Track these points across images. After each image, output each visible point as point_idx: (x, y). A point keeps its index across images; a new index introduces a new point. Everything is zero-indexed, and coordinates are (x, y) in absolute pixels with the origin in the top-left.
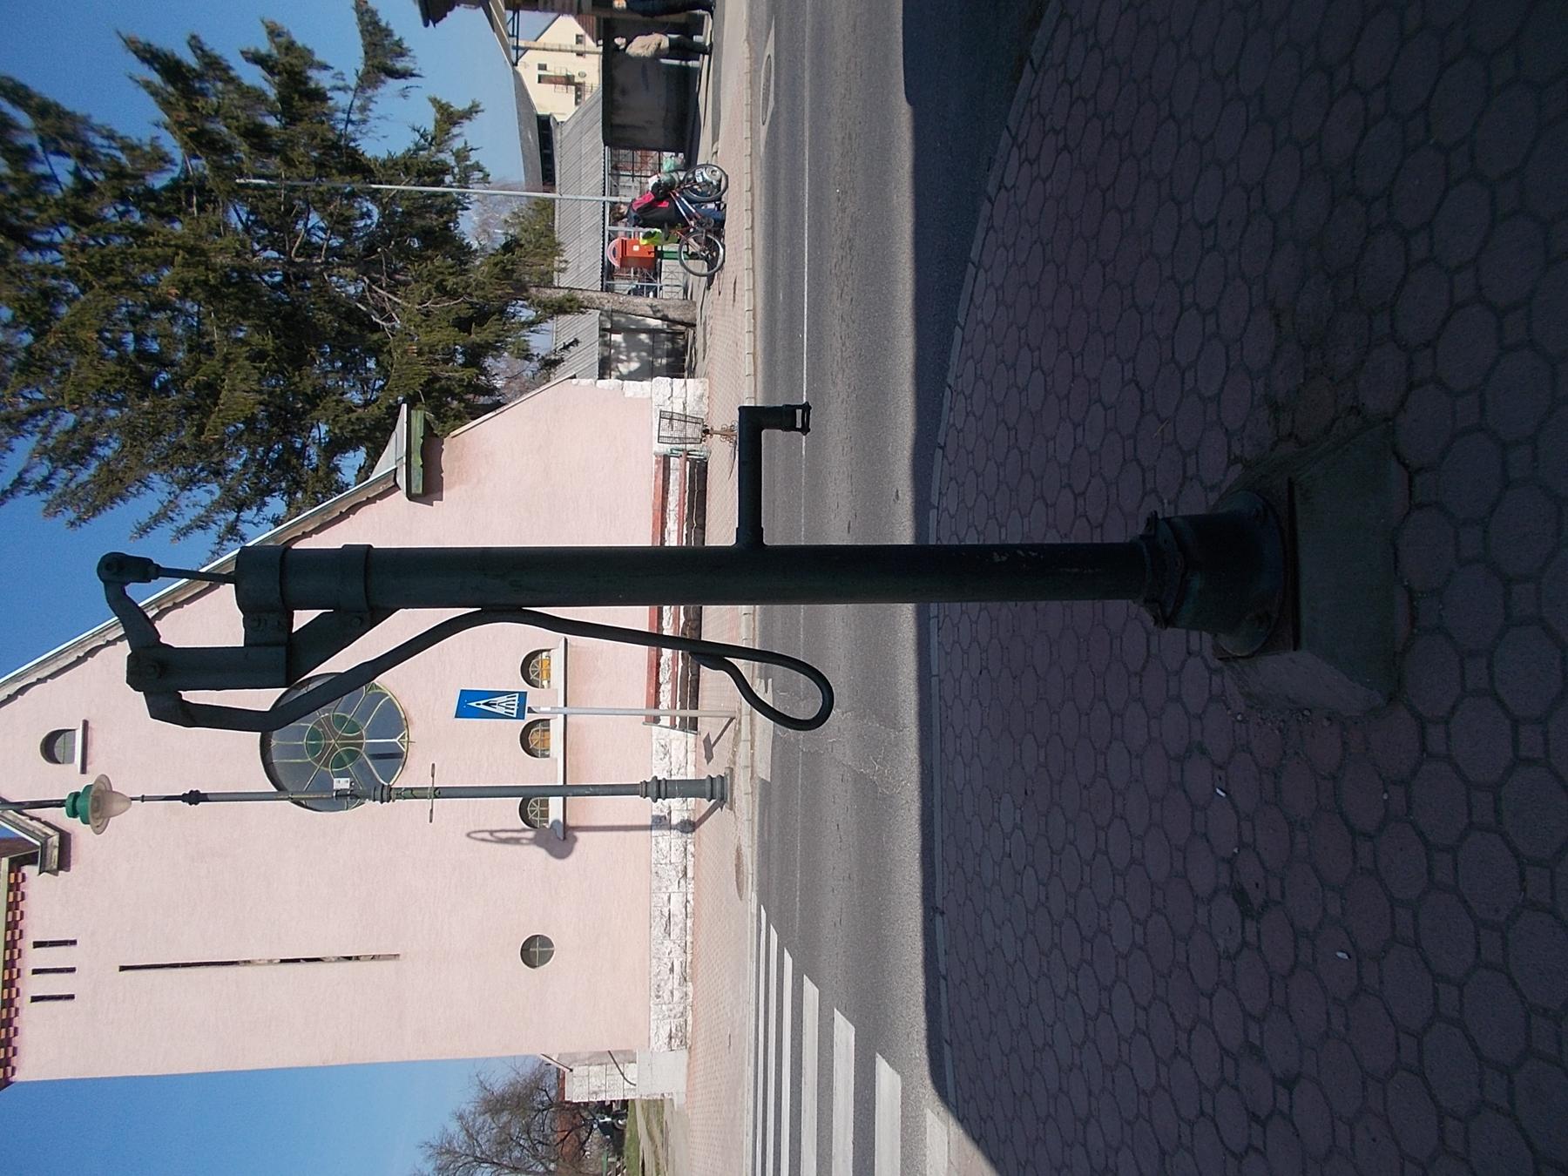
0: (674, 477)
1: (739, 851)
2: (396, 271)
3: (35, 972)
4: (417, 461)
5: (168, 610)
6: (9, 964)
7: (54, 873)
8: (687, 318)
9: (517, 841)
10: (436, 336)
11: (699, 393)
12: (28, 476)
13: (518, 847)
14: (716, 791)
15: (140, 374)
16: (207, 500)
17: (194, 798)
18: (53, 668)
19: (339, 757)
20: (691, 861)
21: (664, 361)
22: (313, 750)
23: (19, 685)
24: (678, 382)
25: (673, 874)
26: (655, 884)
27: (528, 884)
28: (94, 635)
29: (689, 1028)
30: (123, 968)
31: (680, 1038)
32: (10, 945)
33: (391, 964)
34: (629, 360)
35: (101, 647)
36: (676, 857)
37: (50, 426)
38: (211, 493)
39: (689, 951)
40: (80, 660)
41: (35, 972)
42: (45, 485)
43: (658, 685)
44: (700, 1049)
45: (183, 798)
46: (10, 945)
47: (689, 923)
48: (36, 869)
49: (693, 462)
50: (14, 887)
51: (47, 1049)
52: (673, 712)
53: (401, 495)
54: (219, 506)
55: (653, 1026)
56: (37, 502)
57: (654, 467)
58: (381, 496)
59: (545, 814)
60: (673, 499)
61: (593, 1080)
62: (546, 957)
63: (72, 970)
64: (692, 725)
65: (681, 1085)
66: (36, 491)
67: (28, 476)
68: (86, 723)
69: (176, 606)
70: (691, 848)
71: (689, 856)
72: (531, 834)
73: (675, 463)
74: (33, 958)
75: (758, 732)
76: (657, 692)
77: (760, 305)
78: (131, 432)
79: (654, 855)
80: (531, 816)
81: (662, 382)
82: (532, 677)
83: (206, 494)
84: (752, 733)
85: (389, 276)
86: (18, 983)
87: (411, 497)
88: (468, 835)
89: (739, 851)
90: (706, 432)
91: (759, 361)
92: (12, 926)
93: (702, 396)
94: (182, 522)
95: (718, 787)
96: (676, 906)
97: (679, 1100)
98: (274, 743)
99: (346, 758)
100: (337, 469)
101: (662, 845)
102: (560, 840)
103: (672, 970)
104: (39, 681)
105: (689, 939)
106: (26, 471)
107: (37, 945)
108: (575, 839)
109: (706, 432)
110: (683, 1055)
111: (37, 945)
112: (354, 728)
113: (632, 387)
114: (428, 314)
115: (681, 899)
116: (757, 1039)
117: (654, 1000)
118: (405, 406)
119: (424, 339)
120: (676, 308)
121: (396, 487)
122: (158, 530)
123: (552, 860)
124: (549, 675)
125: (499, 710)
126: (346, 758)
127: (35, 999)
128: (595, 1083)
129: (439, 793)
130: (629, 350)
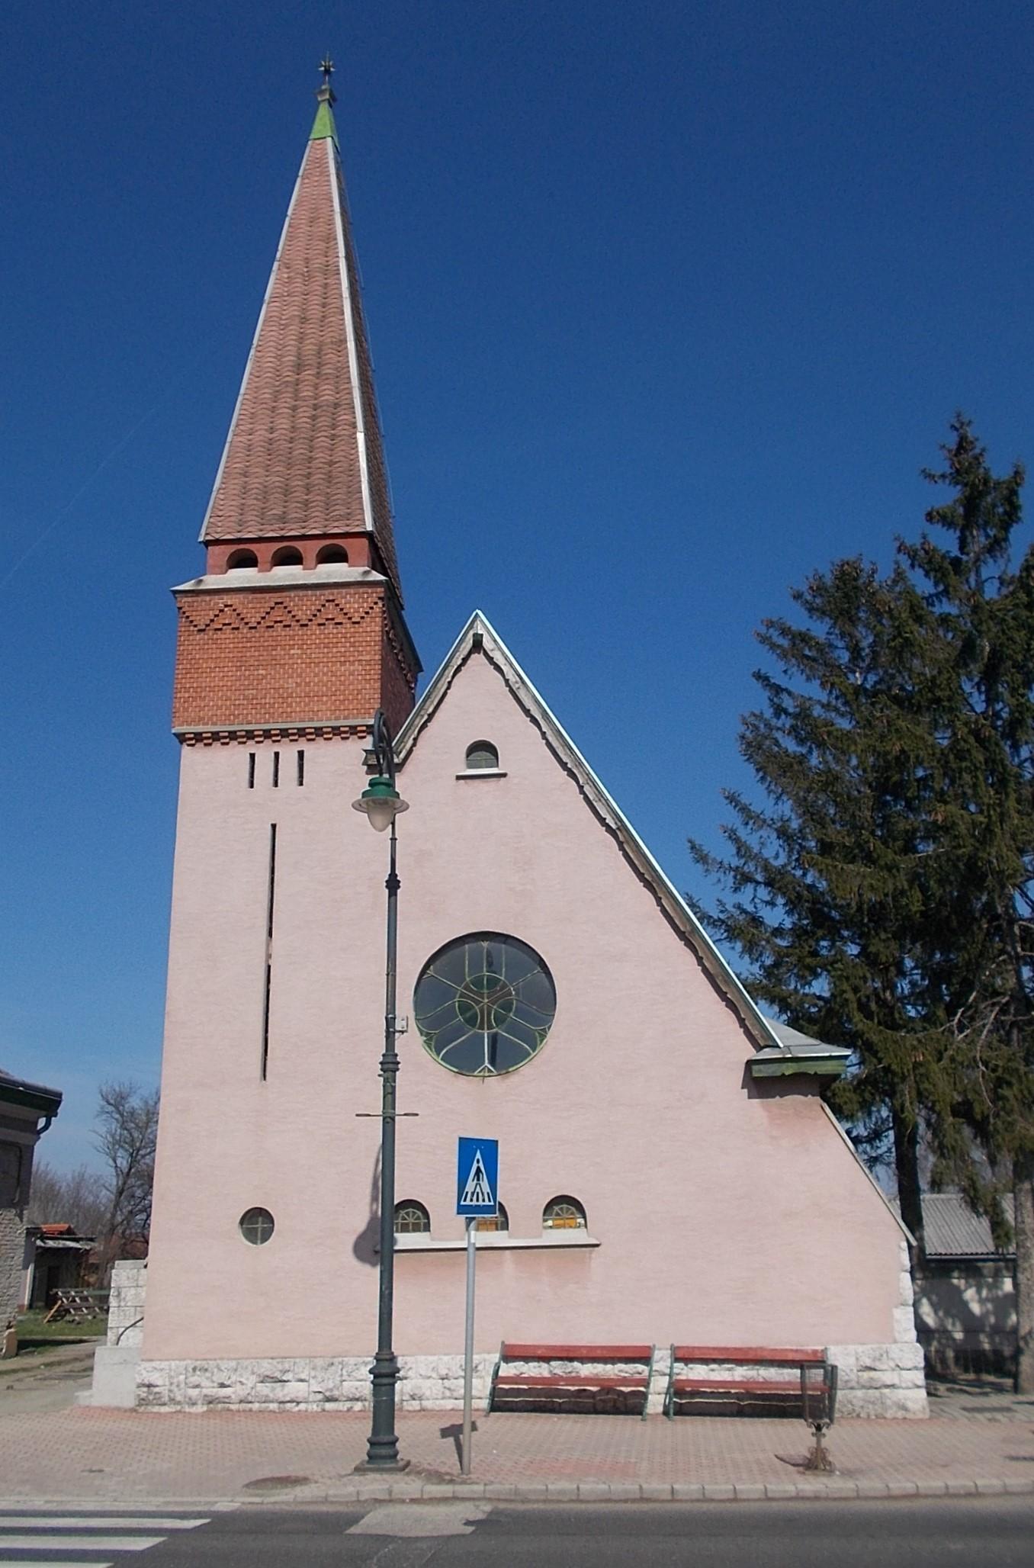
2: (1020, 1030)
3: (277, 754)
4: (789, 1069)
5: (616, 837)
6: (284, 733)
11: (909, 1405)
12: (784, 696)
13: (368, 1199)
14: (382, 1449)
15: (890, 782)
16: (768, 853)
17: (393, 884)
19: (470, 1008)
20: (343, 1406)
21: (987, 1346)
22: (478, 982)
23: (539, 717)
24: (919, 1377)
26: (319, 1362)
28: (588, 774)
29: (156, 1409)
30: (274, 826)
31: (149, 1395)
32: (302, 733)
33: (259, 1072)
34: (981, 1301)
35: (577, 782)
36: (349, 1387)
37: (836, 710)
38: (777, 856)
39: (243, 1406)
40: (564, 765)
41: (277, 754)
42: (779, 711)
43: (547, 1359)
46: (302, 733)
47: (273, 1406)
48: (370, 748)
50: (354, 730)
51: (207, 775)
53: (751, 1053)
54: (766, 867)
55: (164, 1365)
57: (810, 1348)
58: (748, 1034)
59: (405, 1229)
61: (133, 1291)
62: (266, 1235)
63: (276, 784)
64: (499, 1403)
65: (96, 1402)
67: (784, 696)
68: (504, 775)
69: (620, 844)
70: (358, 1406)
71: (348, 1404)
74: (289, 752)
75: (417, 1509)
77: (978, 1504)
78: (830, 781)
79: (352, 1361)
81: (915, 1355)
82: (556, 1208)
85: (1013, 1024)
86: (268, 742)
87: (750, 1064)
92: (319, 732)
93: (905, 1408)
94: (743, 833)
95: (383, 1451)
96: (294, 1389)
97: (84, 1397)
98: (485, 944)
99: (468, 1015)
100: (816, 976)
103: (222, 1385)
104: (543, 734)
105: (256, 1406)
106: (790, 693)
107: (301, 754)
108: (374, 1265)
110: (130, 1402)
111: (301, 754)
112: (500, 1020)
113: (905, 1319)
117: (191, 1364)
121: (759, 1048)
122: (734, 813)
124: (558, 1227)
125: (470, 1186)
126: (468, 1015)
129: (389, 1122)
130: (995, 1300)
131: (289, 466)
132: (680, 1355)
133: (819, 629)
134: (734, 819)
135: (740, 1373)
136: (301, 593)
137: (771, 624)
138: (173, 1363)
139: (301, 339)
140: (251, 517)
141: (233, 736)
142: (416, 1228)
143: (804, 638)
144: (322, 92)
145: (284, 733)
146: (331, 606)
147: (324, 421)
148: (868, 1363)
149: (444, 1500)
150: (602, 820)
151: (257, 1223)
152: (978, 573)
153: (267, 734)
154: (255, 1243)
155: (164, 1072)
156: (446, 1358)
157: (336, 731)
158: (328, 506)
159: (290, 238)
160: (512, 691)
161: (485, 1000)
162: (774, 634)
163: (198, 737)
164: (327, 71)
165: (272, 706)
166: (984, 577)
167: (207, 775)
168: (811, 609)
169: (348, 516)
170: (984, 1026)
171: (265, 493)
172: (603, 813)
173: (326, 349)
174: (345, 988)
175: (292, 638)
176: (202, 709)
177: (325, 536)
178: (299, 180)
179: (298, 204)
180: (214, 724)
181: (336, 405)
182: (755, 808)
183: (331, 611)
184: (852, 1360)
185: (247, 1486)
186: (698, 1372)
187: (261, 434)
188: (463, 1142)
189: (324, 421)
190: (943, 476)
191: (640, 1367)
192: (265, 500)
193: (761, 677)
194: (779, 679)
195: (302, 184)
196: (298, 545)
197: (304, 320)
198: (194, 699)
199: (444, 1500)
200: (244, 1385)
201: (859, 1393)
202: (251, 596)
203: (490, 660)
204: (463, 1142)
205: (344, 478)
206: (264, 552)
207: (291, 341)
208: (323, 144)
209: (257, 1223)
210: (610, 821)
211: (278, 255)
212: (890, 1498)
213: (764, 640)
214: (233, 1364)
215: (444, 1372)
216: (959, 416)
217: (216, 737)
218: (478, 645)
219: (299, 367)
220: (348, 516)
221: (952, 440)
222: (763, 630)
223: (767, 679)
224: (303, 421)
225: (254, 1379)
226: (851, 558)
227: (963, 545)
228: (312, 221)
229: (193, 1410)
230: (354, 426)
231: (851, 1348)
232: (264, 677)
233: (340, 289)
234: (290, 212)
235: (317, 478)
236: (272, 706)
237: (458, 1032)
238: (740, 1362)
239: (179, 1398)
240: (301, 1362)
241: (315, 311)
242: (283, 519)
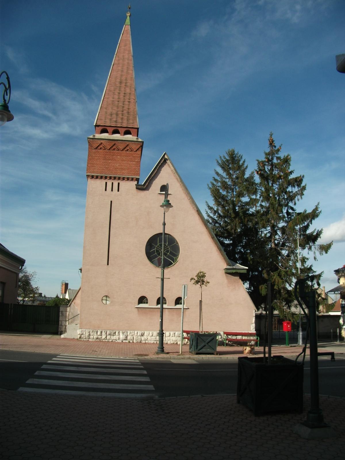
4: (234, 271)
32: (119, 178)
92: (124, 179)
129: (163, 280)
139: (122, 75)
219: (121, 83)
235: (125, 112)
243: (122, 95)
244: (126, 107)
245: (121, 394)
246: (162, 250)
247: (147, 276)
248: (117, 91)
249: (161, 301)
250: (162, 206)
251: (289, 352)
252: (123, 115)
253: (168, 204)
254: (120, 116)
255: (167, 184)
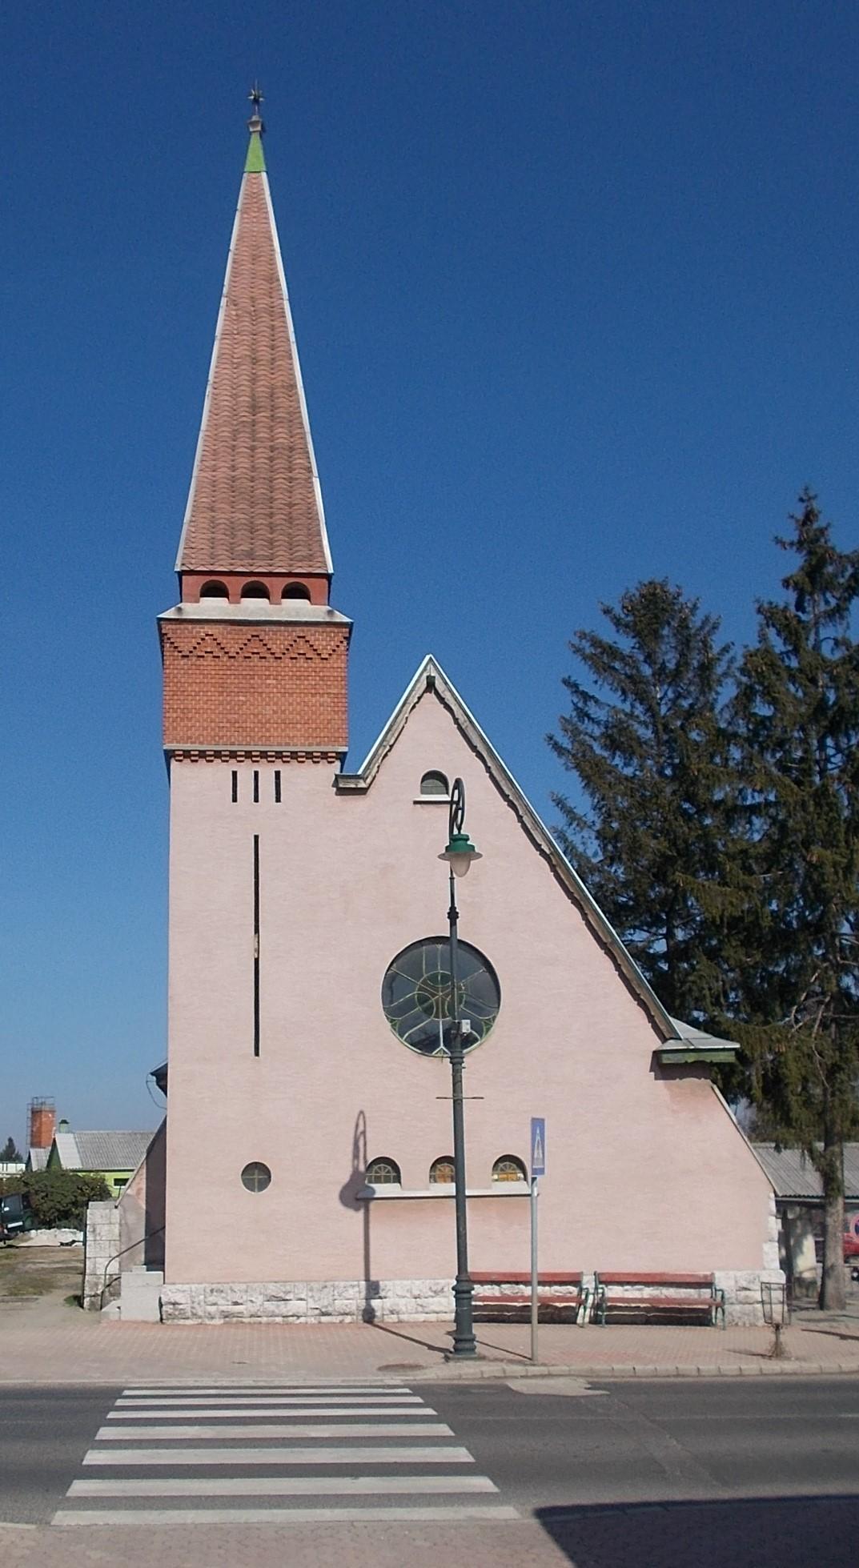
0: (692, 1293)
1: (417, 1367)
2: (838, 1026)
3: (256, 773)
4: (691, 1058)
6: (264, 755)
7: (336, 784)
8: (829, 1300)
9: (356, 1156)
10: (792, 1065)
12: (591, 703)
13: (350, 1156)
18: (498, 778)
20: (336, 1319)
22: (433, 978)
23: (485, 755)
25: (324, 1303)
26: (315, 1286)
27: (317, 1168)
28: (526, 806)
29: (182, 1322)
31: (166, 1314)
32: (279, 755)
40: (505, 797)
41: (256, 773)
43: (498, 1283)
44: (161, 1333)
45: (453, 908)
46: (279, 755)
47: (279, 1319)
49: (708, 1312)
50: (325, 756)
51: (195, 787)
52: (535, 1299)
53: (656, 1044)
55: (186, 1287)
56: (569, 712)
57: (702, 1273)
58: (656, 1027)
59: (378, 1180)
60: (683, 1293)
61: (106, 1228)
62: (249, 1184)
66: (577, 708)
67: (591, 703)
69: (553, 868)
70: (348, 1319)
71: (340, 1318)
72: (362, 1168)
73: (706, 1293)
74: (267, 771)
76: (492, 1283)
79: (342, 1284)
80: (376, 1167)
83: (593, 849)
84: (534, 1376)
87: (657, 1054)
88: (362, 1112)
89: (417, 1367)
90: (777, 1327)
91: (672, 1380)
92: (294, 755)
94: (569, 834)
95: (467, 1345)
98: (440, 946)
101: (351, 1291)
102: (357, 1196)
103: (236, 1303)
105: (264, 1320)
106: (597, 701)
107: (278, 774)
108: (357, 1209)
109: (777, 1327)
111: (278, 774)
114: (810, 1057)
115: (301, 1311)
116: (198, 1388)
118: (737, 1046)
119: (790, 1056)
120: (837, 1289)
121: (664, 1039)
123: (339, 1188)
124: (504, 1180)
127: (235, 774)
128: (103, 1230)
129: (458, 1104)
131: (252, 504)
132: (603, 1279)
133: (626, 643)
134: (561, 820)
135: (648, 1292)
136: (275, 628)
137: (583, 636)
138: (193, 1287)
139: (254, 380)
140: (220, 550)
141: (218, 754)
142: (387, 1180)
143: (612, 652)
144: (254, 124)
145: (264, 755)
146: (301, 642)
147: (280, 463)
148: (745, 1284)
149: (543, 1376)
150: (538, 846)
151: (257, 1175)
152: (817, 633)
153: (248, 755)
154: (252, 1190)
155: (170, 1047)
156: (418, 1282)
157: (309, 755)
158: (291, 546)
159: (235, 274)
160: (460, 728)
161: (441, 996)
162: (586, 644)
163: (187, 754)
164: (256, 101)
165: (252, 730)
166: (822, 637)
167: (195, 787)
168: (617, 622)
169: (310, 558)
170: (814, 1020)
171: (232, 529)
172: (539, 840)
173: (279, 392)
174: (337, 981)
175: (268, 668)
176: (190, 728)
177: (290, 575)
178: (238, 214)
179: (240, 238)
180: (201, 743)
181: (291, 449)
182: (579, 811)
183: (303, 648)
184: (732, 1283)
185: (380, 1369)
186: (614, 1292)
187: (223, 473)
188: (533, 1119)
189: (280, 463)
190: (792, 544)
191: (571, 1288)
192: (234, 536)
193: (573, 686)
194: (592, 690)
195: (242, 218)
196: (265, 580)
197: (255, 361)
198: (182, 720)
199: (543, 1376)
200: (254, 1303)
201: (738, 1307)
202: (229, 628)
203: (442, 700)
204: (533, 1119)
205: (304, 520)
206: (235, 585)
207: (244, 380)
208: (257, 181)
209: (257, 1175)
210: (544, 847)
211: (225, 290)
212: (842, 1373)
213: (578, 650)
214: (244, 1287)
215: (416, 1293)
216: (806, 489)
217: (202, 754)
218: (431, 686)
219: (254, 408)
220: (310, 558)
221: (799, 512)
222: (576, 641)
223: (576, 686)
224: (261, 460)
225: (261, 1298)
226: (658, 580)
227: (800, 606)
228: (254, 258)
229: (213, 1322)
230: (309, 470)
231: (732, 1273)
232: (244, 703)
233: (286, 332)
234: (232, 247)
235: (279, 518)
236: (252, 730)
237: (417, 1020)
238: (647, 1284)
239: (200, 1313)
240: (300, 1285)
241: (264, 353)
242: (250, 555)
243: (262, 454)
244: (281, 498)
245: (318, 1511)
246: (441, 996)
247: (403, 1100)
248: (244, 441)
249: (451, 1166)
250: (441, 857)
251: (562, 1380)
252: (272, 528)
253: (459, 849)
254: (264, 532)
255: (480, 856)
